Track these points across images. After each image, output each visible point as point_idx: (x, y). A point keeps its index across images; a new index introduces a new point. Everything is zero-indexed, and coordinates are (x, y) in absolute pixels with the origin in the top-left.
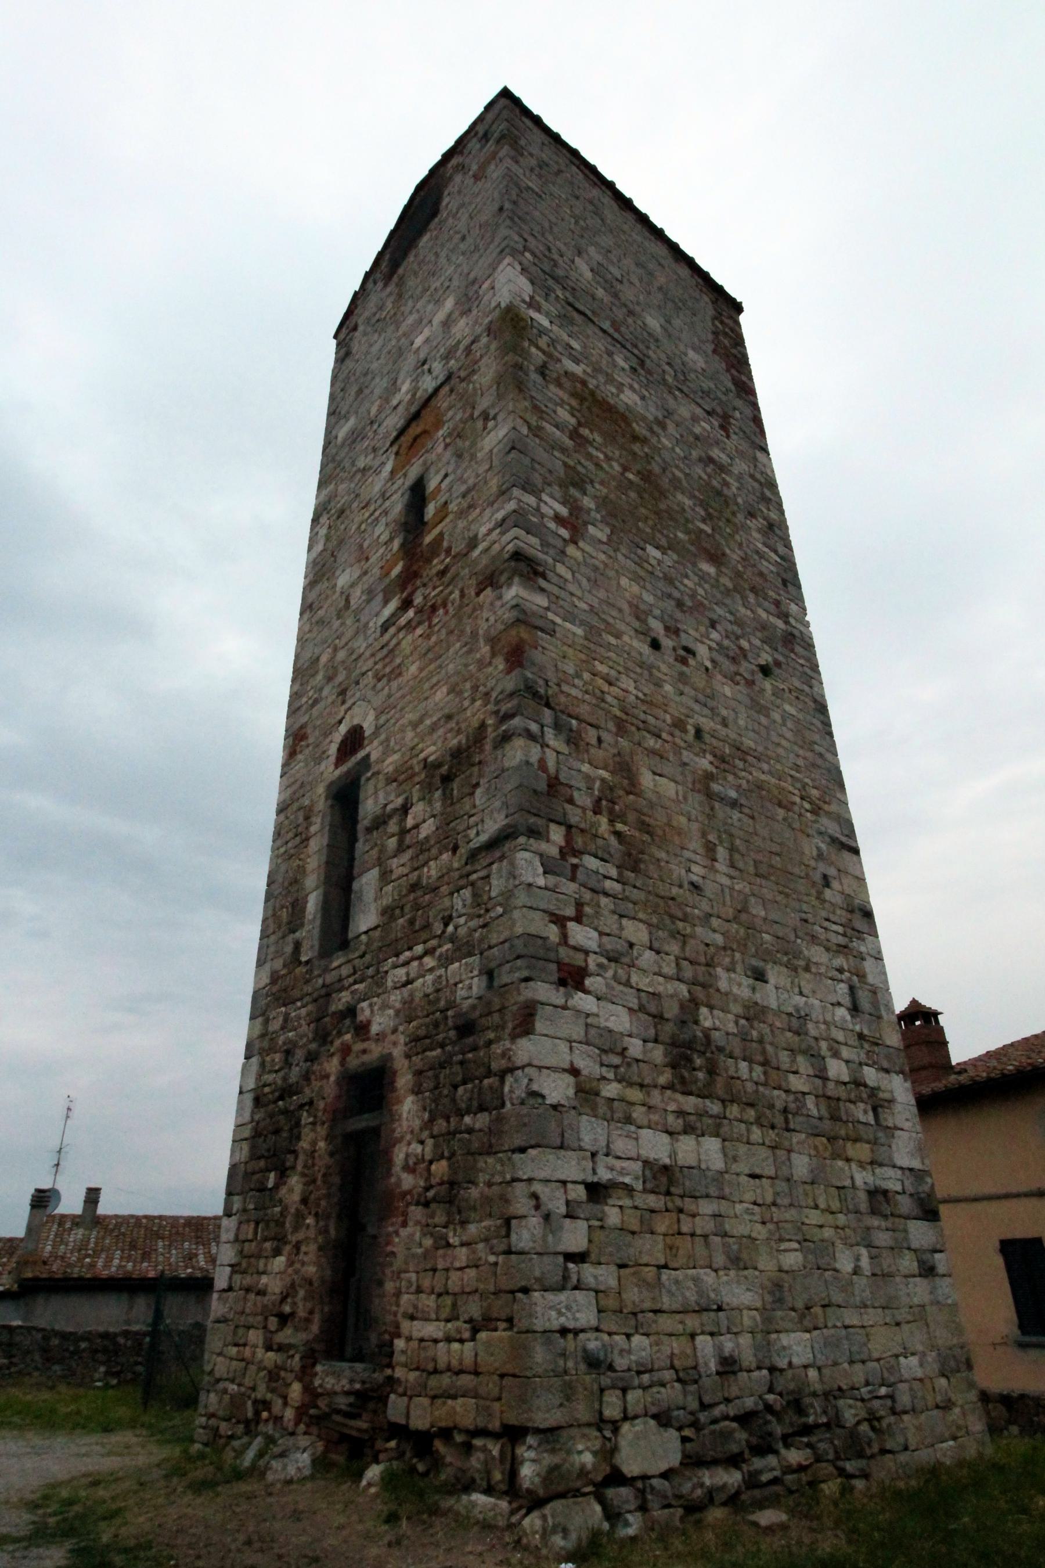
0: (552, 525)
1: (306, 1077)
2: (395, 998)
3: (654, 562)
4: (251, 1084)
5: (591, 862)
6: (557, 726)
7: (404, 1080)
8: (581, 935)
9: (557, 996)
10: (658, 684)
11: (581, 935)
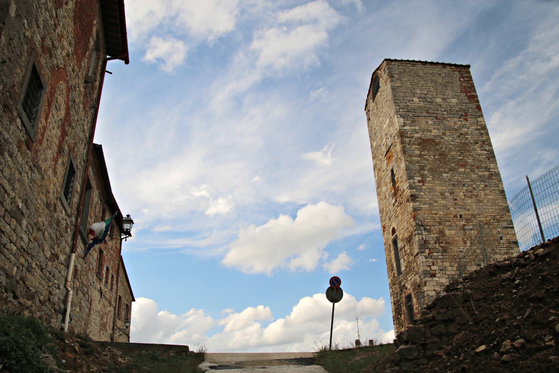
0: (418, 184)
1: (400, 298)
2: (410, 282)
3: (445, 178)
4: (392, 301)
5: (435, 254)
6: (425, 229)
7: (413, 296)
8: (433, 268)
10: (449, 209)
11: (433, 268)
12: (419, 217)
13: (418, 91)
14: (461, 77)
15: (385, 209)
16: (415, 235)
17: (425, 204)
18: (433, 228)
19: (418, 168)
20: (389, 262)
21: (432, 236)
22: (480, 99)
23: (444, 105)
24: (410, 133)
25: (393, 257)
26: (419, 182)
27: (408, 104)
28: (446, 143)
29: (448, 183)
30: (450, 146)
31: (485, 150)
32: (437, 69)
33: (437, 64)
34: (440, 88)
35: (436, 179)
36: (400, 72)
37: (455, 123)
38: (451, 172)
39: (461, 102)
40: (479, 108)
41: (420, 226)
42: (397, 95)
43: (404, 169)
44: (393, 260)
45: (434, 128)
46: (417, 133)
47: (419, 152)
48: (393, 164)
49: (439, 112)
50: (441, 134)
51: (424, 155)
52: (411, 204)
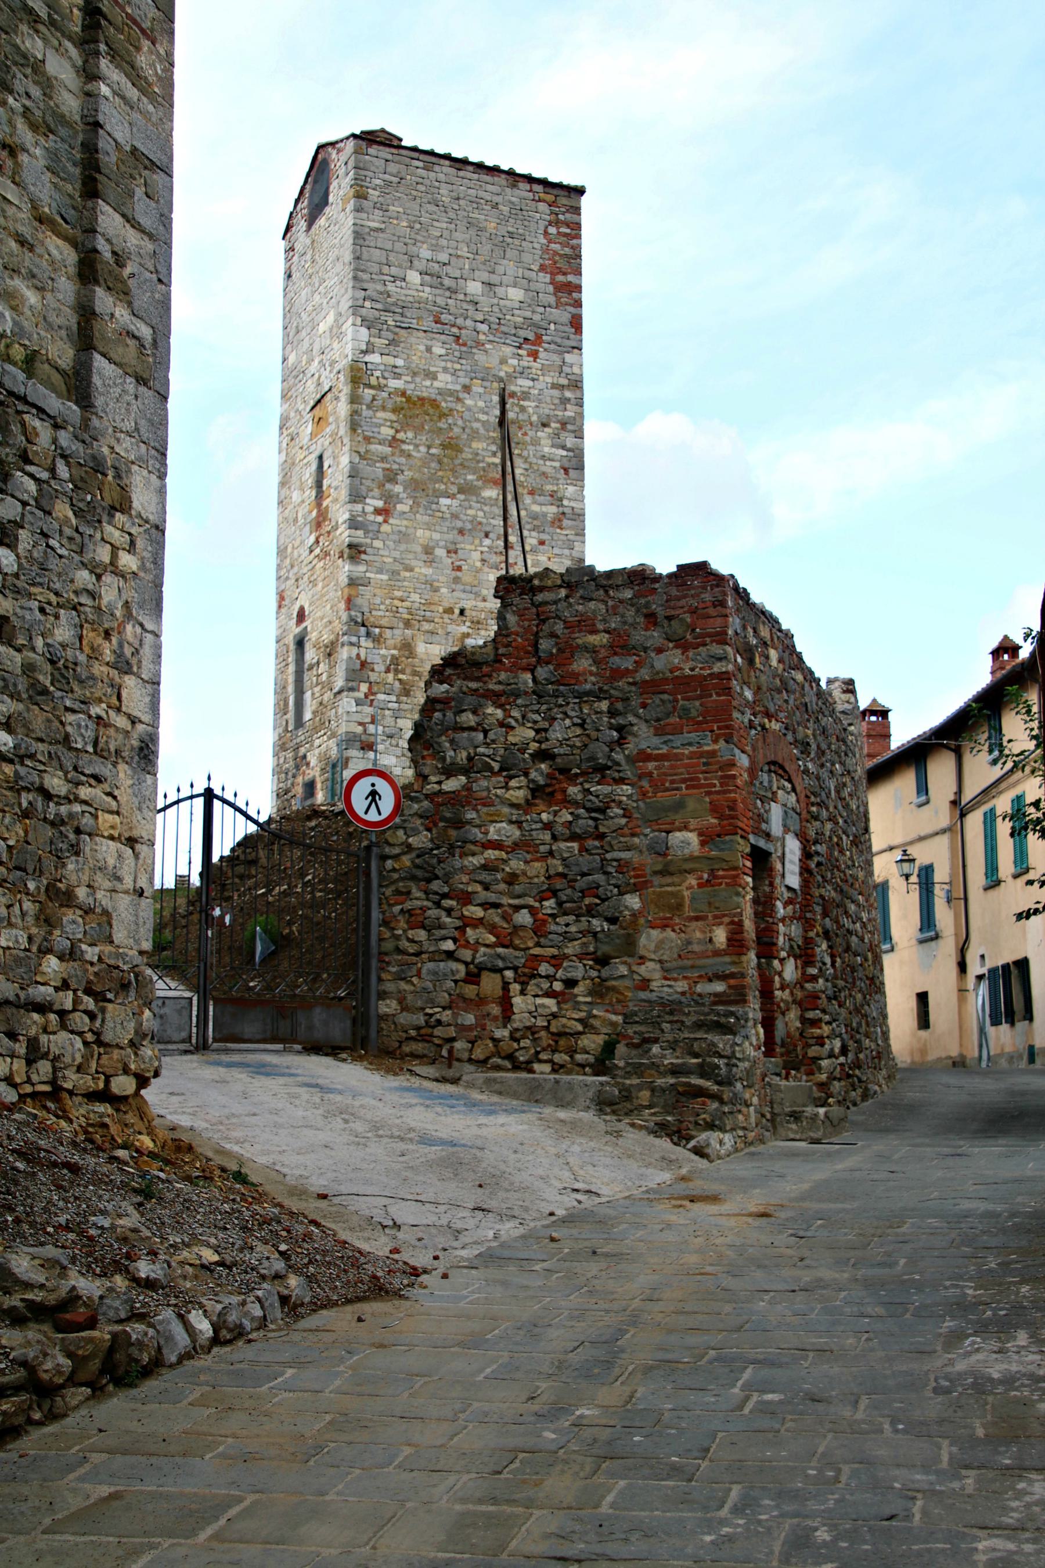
0: (371, 517)
1: (293, 784)
2: (317, 751)
3: (444, 509)
5: (381, 697)
6: (368, 634)
7: (319, 786)
9: (360, 754)
10: (436, 590)
12: (359, 601)
13: (425, 253)
14: (550, 223)
15: (289, 550)
16: (343, 645)
17: (380, 571)
18: (388, 633)
19: (380, 473)
20: (280, 689)
21: (383, 652)
22: (586, 296)
23: (485, 303)
24: (378, 373)
25: (291, 679)
26: (378, 511)
27: (391, 287)
28: (467, 415)
29: (447, 524)
30: (476, 425)
31: (564, 447)
32: (494, 186)
33: (495, 170)
34: (485, 248)
35: (421, 510)
36: (388, 184)
37: (503, 361)
38: (462, 497)
39: (534, 300)
40: (576, 324)
41: (360, 624)
42: (365, 256)
43: (347, 470)
44: (291, 689)
45: (445, 370)
46: (398, 376)
47: (392, 432)
48: (323, 443)
49: (469, 323)
50: (458, 387)
51: (403, 442)
52: (347, 568)
